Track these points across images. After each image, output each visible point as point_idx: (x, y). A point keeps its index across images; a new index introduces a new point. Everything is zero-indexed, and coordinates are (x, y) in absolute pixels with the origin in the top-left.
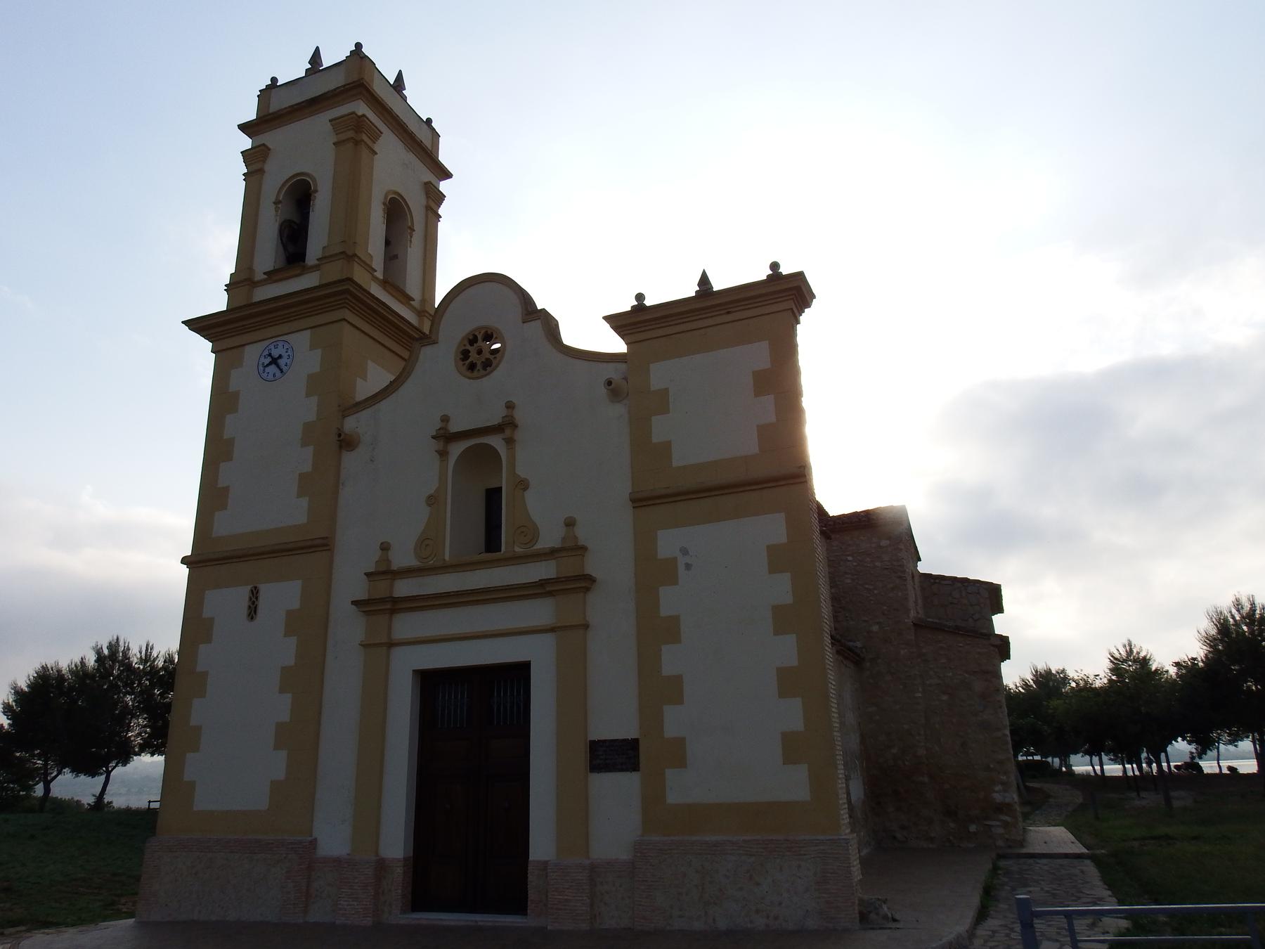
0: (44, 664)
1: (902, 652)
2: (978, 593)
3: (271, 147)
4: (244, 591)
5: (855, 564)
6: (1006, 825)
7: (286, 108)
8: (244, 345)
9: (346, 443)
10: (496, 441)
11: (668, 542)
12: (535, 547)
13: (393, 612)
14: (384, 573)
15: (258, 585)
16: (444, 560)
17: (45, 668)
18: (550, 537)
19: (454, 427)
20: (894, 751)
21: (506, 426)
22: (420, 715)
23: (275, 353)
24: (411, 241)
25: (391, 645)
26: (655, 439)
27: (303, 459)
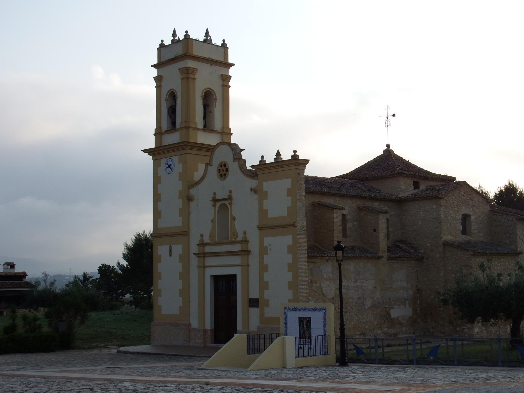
0: (138, 233)
1: (437, 256)
2: (512, 221)
3: (162, 75)
4: (168, 247)
5: (423, 215)
6: (469, 328)
7: (165, 61)
8: (161, 159)
9: (190, 199)
10: (226, 203)
12: (237, 239)
13: (204, 257)
14: (202, 244)
15: (172, 245)
16: (216, 241)
17: (139, 235)
18: (240, 237)
19: (218, 197)
20: (432, 297)
21: (230, 198)
23: (170, 163)
24: (216, 105)
25: (204, 267)
26: (181, 263)
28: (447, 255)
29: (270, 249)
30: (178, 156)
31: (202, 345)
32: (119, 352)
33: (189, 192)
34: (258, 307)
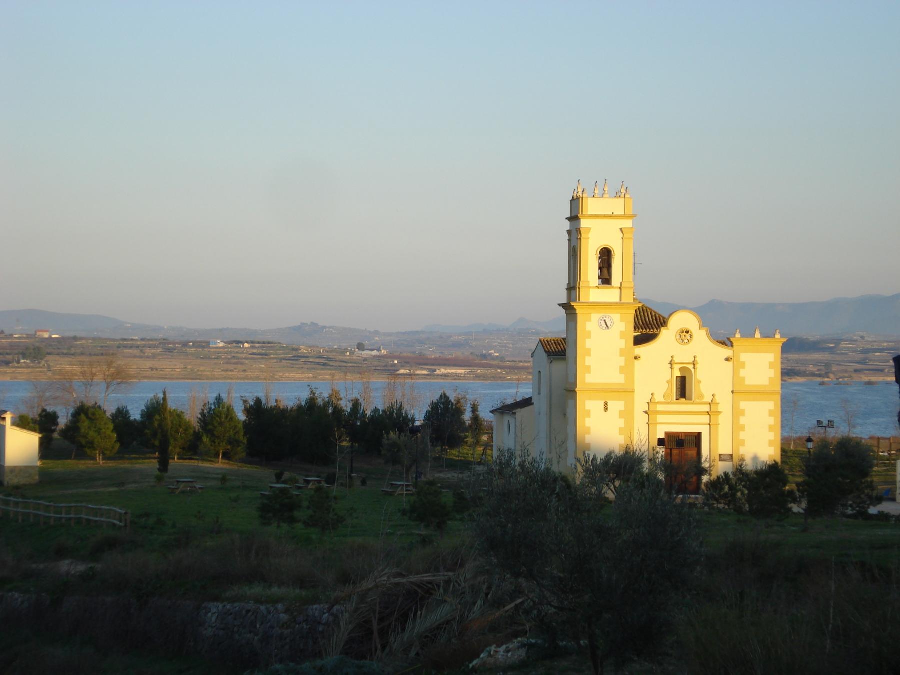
11: (743, 405)
15: (608, 402)
22: (644, 344)
27: (622, 361)
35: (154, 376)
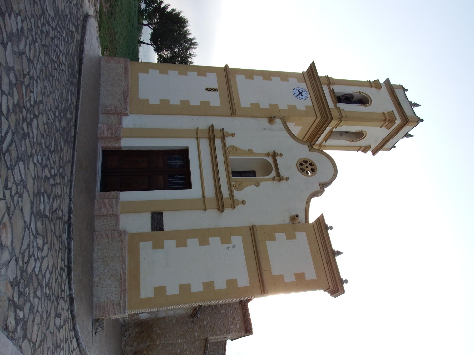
4: (216, 86)
5: (230, 314)
7: (396, 95)
9: (271, 120)
10: (273, 174)
12: (234, 190)
14: (223, 135)
15: (218, 91)
18: (238, 195)
19: (278, 159)
20: (159, 331)
21: (279, 178)
23: (303, 94)
27: (265, 105)
28: (197, 342)
29: (228, 248)
30: (312, 105)
31: (99, 135)
32: (87, 16)
33: (278, 118)
34: (153, 230)
35: (48, 28)
